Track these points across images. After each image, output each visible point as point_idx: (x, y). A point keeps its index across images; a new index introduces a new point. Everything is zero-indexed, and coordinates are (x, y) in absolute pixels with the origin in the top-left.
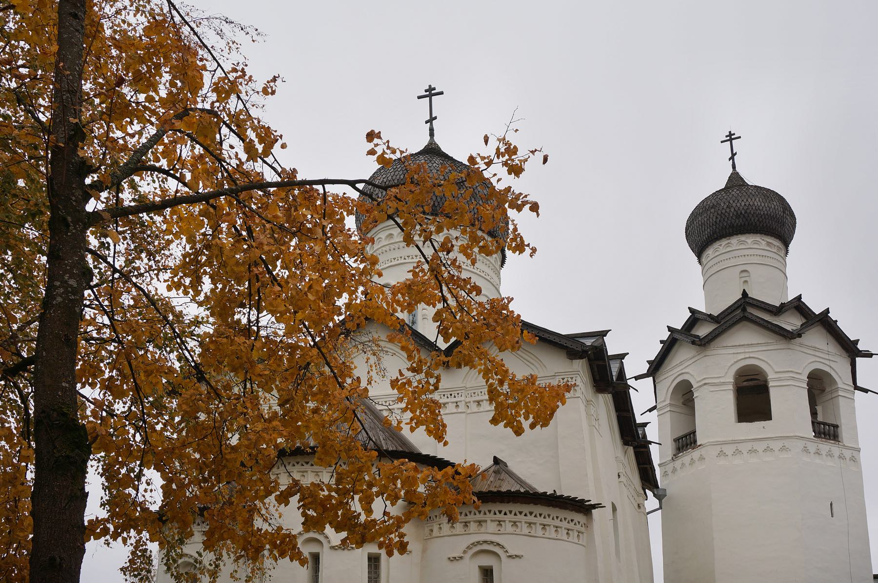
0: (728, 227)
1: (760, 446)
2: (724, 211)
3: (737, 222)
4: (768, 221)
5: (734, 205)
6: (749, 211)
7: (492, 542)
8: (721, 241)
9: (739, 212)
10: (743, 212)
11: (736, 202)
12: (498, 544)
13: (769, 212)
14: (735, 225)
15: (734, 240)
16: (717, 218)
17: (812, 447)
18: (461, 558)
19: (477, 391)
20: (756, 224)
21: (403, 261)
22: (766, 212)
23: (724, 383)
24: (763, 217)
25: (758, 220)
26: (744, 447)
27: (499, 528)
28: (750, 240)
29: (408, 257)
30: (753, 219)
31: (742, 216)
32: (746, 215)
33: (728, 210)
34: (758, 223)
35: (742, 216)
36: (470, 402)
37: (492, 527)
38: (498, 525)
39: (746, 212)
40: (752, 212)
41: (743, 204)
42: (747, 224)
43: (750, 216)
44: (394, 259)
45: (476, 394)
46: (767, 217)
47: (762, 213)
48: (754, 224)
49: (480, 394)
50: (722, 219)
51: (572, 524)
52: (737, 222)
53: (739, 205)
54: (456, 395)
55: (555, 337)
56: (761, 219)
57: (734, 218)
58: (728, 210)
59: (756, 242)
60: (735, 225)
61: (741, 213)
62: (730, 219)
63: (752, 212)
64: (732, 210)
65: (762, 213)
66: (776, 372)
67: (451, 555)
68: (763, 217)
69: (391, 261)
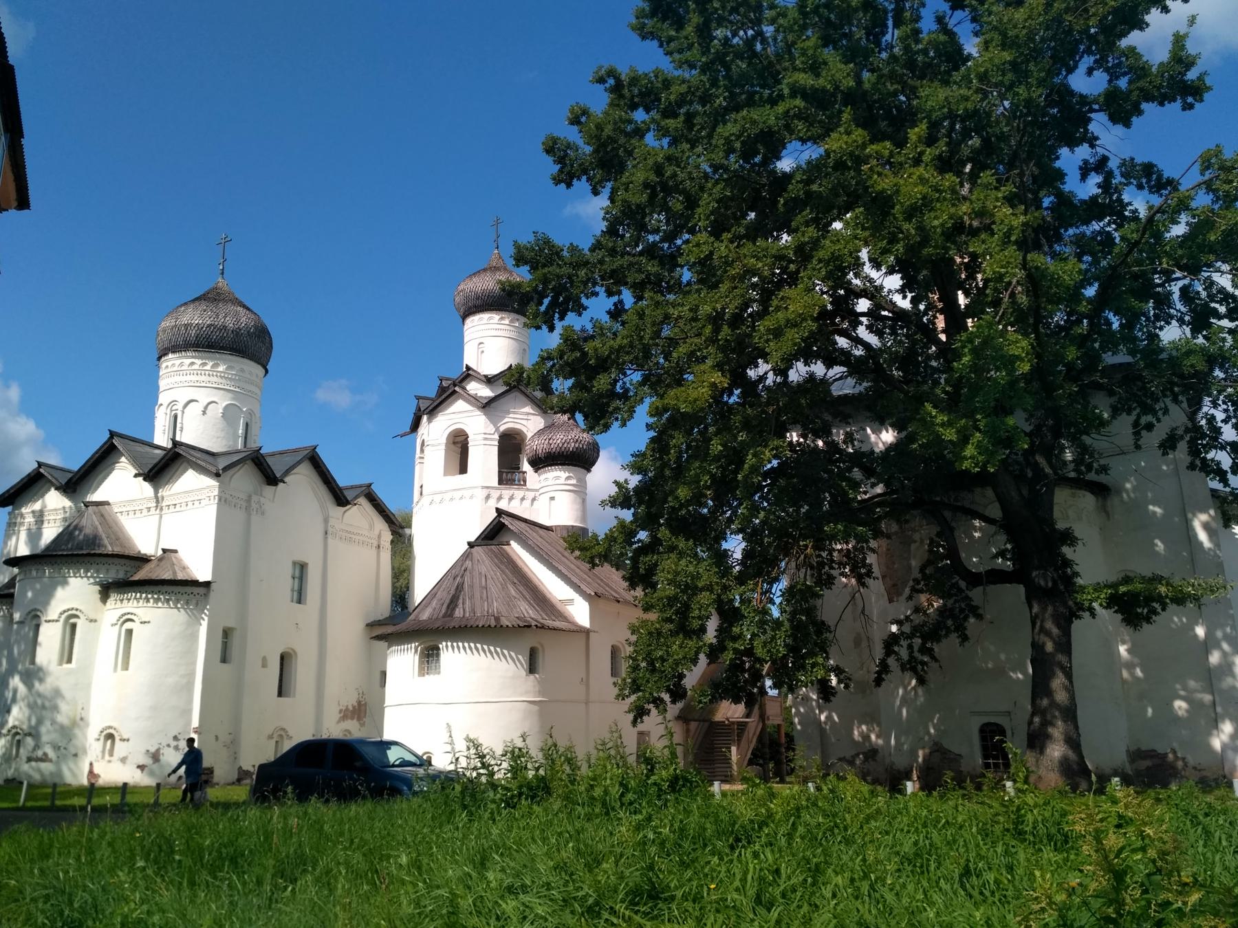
1: (457, 495)
17: (495, 494)
26: (447, 496)
28: (485, 316)
51: (192, 596)
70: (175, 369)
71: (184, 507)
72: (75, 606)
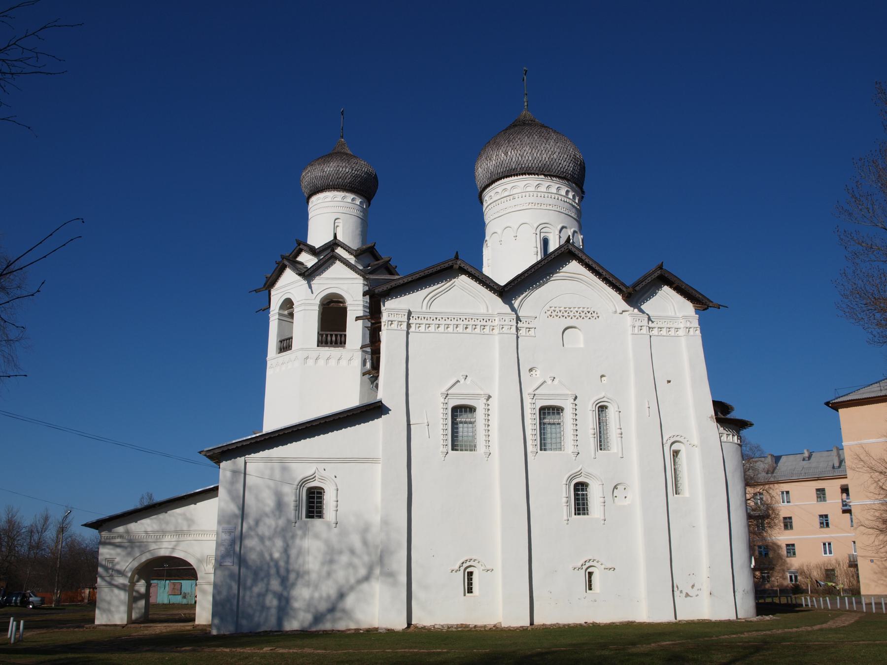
23: (359, 301)
28: (321, 196)
54: (459, 319)
66: (298, 301)
70: (506, 194)
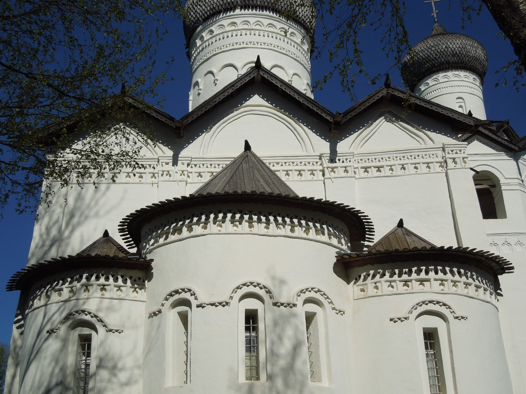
0: (445, 63)
2: (442, 50)
3: (453, 59)
4: (474, 61)
5: (451, 46)
6: (462, 52)
7: (438, 303)
8: (439, 74)
9: (455, 52)
10: (458, 52)
11: (453, 44)
12: (444, 305)
13: (476, 55)
14: (451, 61)
15: (450, 74)
16: (436, 55)
18: (160, 312)
19: (379, 157)
20: (466, 63)
21: (245, 46)
22: (473, 55)
24: (472, 58)
25: (468, 60)
27: (442, 287)
28: (462, 74)
29: (250, 43)
30: (464, 58)
31: (456, 55)
32: (460, 55)
33: (446, 50)
34: (468, 62)
35: (456, 55)
36: (358, 168)
37: (448, 286)
38: (440, 284)
39: (460, 53)
40: (464, 53)
41: (458, 46)
42: (460, 61)
43: (463, 56)
44: (236, 44)
45: (364, 160)
46: (474, 58)
47: (471, 55)
48: (465, 63)
49: (367, 161)
50: (441, 56)
52: (453, 59)
53: (454, 46)
55: (448, 112)
56: (470, 60)
57: (451, 56)
58: (446, 50)
59: (466, 77)
60: (451, 61)
61: (456, 53)
62: (447, 56)
63: (464, 53)
64: (450, 50)
65: (471, 55)
67: (395, 316)
68: (472, 58)
69: (227, 47)
71: (398, 170)
72: (318, 286)
